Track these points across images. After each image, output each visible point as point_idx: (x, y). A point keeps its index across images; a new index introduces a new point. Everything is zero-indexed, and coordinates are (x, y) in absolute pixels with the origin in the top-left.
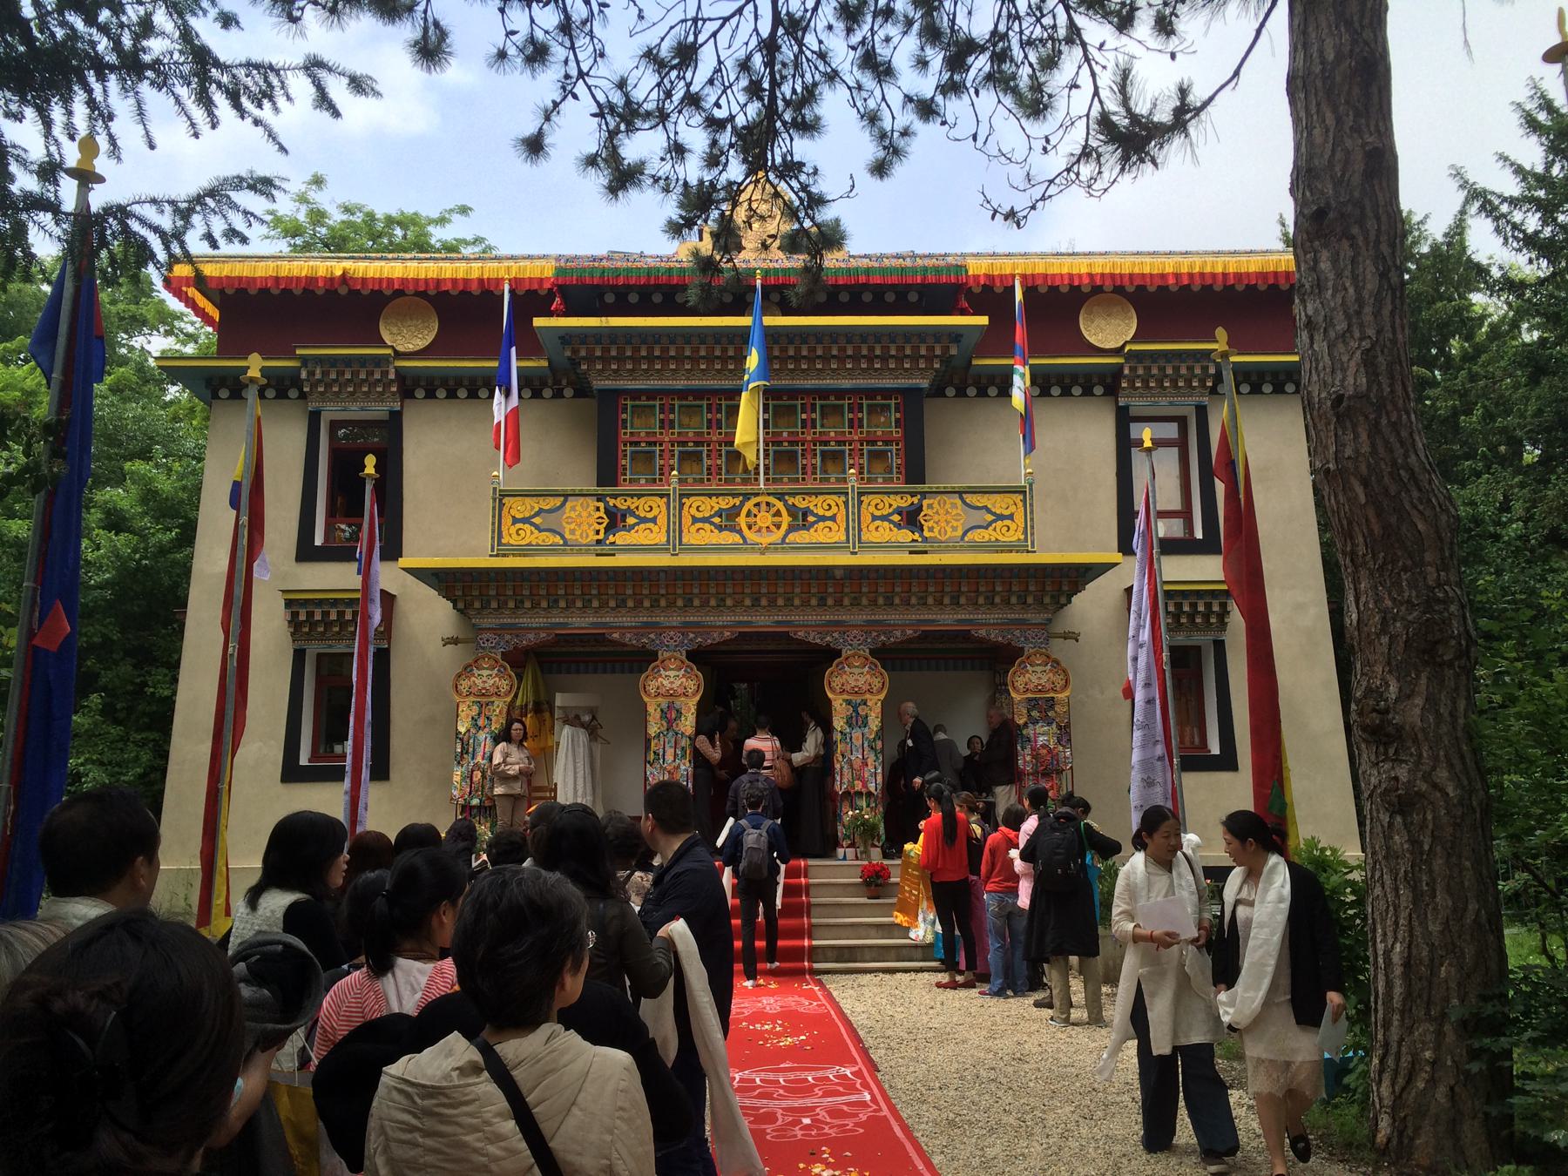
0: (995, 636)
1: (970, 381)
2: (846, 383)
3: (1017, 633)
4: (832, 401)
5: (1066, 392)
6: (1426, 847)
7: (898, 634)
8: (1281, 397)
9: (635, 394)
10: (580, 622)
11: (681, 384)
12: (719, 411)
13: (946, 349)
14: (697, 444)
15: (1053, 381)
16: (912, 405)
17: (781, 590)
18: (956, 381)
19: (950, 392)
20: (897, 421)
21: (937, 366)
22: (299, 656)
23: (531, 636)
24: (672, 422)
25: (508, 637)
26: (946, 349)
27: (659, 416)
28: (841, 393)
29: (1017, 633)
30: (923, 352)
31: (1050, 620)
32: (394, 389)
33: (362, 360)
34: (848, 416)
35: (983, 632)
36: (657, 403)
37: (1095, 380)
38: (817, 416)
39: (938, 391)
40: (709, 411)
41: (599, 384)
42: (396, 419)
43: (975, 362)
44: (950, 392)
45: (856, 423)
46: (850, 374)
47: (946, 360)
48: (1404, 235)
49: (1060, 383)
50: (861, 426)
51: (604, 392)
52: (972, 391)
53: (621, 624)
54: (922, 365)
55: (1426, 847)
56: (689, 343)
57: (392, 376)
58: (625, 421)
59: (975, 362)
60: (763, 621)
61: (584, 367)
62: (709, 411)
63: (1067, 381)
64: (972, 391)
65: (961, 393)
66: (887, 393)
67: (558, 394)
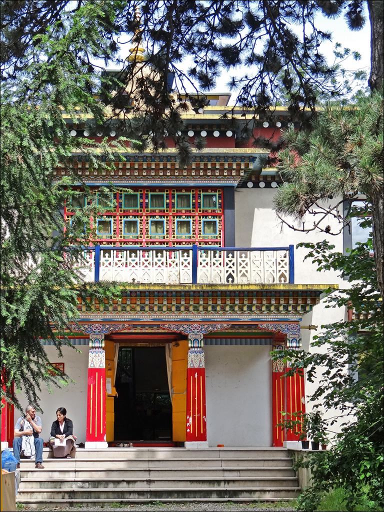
0: (271, 327)
1: (261, 179)
2: (191, 183)
3: (283, 326)
4: (184, 193)
7: (219, 326)
13: (247, 166)
16: (227, 196)
17: (147, 302)
18: (253, 179)
19: (250, 185)
21: (242, 174)
24: (147, 204)
26: (247, 166)
29: (283, 326)
30: (153, 167)
31: (301, 319)
35: (264, 326)
39: (243, 185)
43: (263, 170)
44: (250, 185)
46: (146, 178)
48: (151, 35)
50: (147, 207)
52: (262, 184)
54: (217, 174)
64: (262, 184)
65: (256, 185)
66: (214, 189)
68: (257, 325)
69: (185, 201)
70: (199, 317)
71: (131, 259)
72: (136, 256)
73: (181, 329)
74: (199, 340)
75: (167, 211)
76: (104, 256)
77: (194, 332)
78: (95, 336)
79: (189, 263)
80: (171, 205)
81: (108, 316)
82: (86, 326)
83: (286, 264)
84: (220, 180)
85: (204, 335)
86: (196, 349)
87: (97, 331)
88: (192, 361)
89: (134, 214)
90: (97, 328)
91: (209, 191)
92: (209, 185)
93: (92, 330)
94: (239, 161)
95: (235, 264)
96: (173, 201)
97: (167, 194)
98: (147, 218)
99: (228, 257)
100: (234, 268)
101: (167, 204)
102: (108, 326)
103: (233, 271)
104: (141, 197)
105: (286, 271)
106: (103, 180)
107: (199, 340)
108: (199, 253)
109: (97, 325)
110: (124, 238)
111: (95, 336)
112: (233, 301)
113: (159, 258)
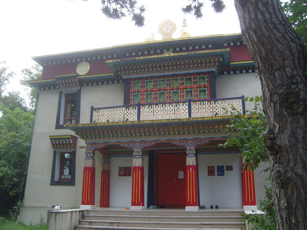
1: (231, 69)
2: (191, 72)
4: (202, 76)
5: (103, 84)
6: (294, 206)
7: (203, 142)
8: (108, 85)
9: (134, 79)
10: (112, 141)
11: (146, 75)
12: (170, 81)
14: (191, 88)
15: (243, 69)
19: (226, 73)
20: (207, 81)
22: (55, 153)
23: (100, 145)
24: (144, 86)
25: (94, 146)
27: (141, 85)
28: (191, 74)
32: (78, 84)
33: (71, 77)
34: (193, 81)
36: (206, 76)
37: (243, 69)
38: (184, 81)
40: (141, 83)
41: (124, 77)
42: (79, 91)
44: (226, 73)
45: (195, 82)
47: (219, 62)
49: (233, 70)
51: (126, 79)
52: (232, 72)
53: (123, 141)
55: (294, 206)
56: (200, 59)
57: (77, 81)
58: (132, 87)
59: (231, 64)
60: (163, 139)
61: (120, 73)
62: (167, 81)
63: (235, 69)
64: (232, 72)
65: (229, 73)
66: (204, 73)
67: (118, 82)
68: (119, 145)
69: (190, 81)
70: (138, 139)
71: (177, 107)
72: (218, 104)
73: (182, 144)
74: (193, 150)
75: (154, 88)
76: (142, 108)
77: (189, 146)
78: (137, 150)
79: (136, 113)
80: (195, 82)
81: (143, 139)
82: (185, 143)
83: (240, 106)
84: (206, 68)
85: (195, 147)
86: (191, 155)
87: (137, 147)
88: (188, 161)
89: (176, 88)
90: (137, 145)
91: (202, 75)
92: (200, 71)
93: (187, 144)
94: (214, 57)
95: (212, 108)
96: (183, 81)
97: (193, 77)
98: (197, 88)
99: (126, 110)
100: (129, 116)
101: (180, 83)
102: (143, 144)
103: (218, 111)
104: (167, 81)
105: (186, 113)
106: (147, 74)
107: (193, 150)
108: (192, 103)
109: (138, 144)
110: (199, 99)
111: (137, 150)
112: (214, 126)
113: (128, 111)
